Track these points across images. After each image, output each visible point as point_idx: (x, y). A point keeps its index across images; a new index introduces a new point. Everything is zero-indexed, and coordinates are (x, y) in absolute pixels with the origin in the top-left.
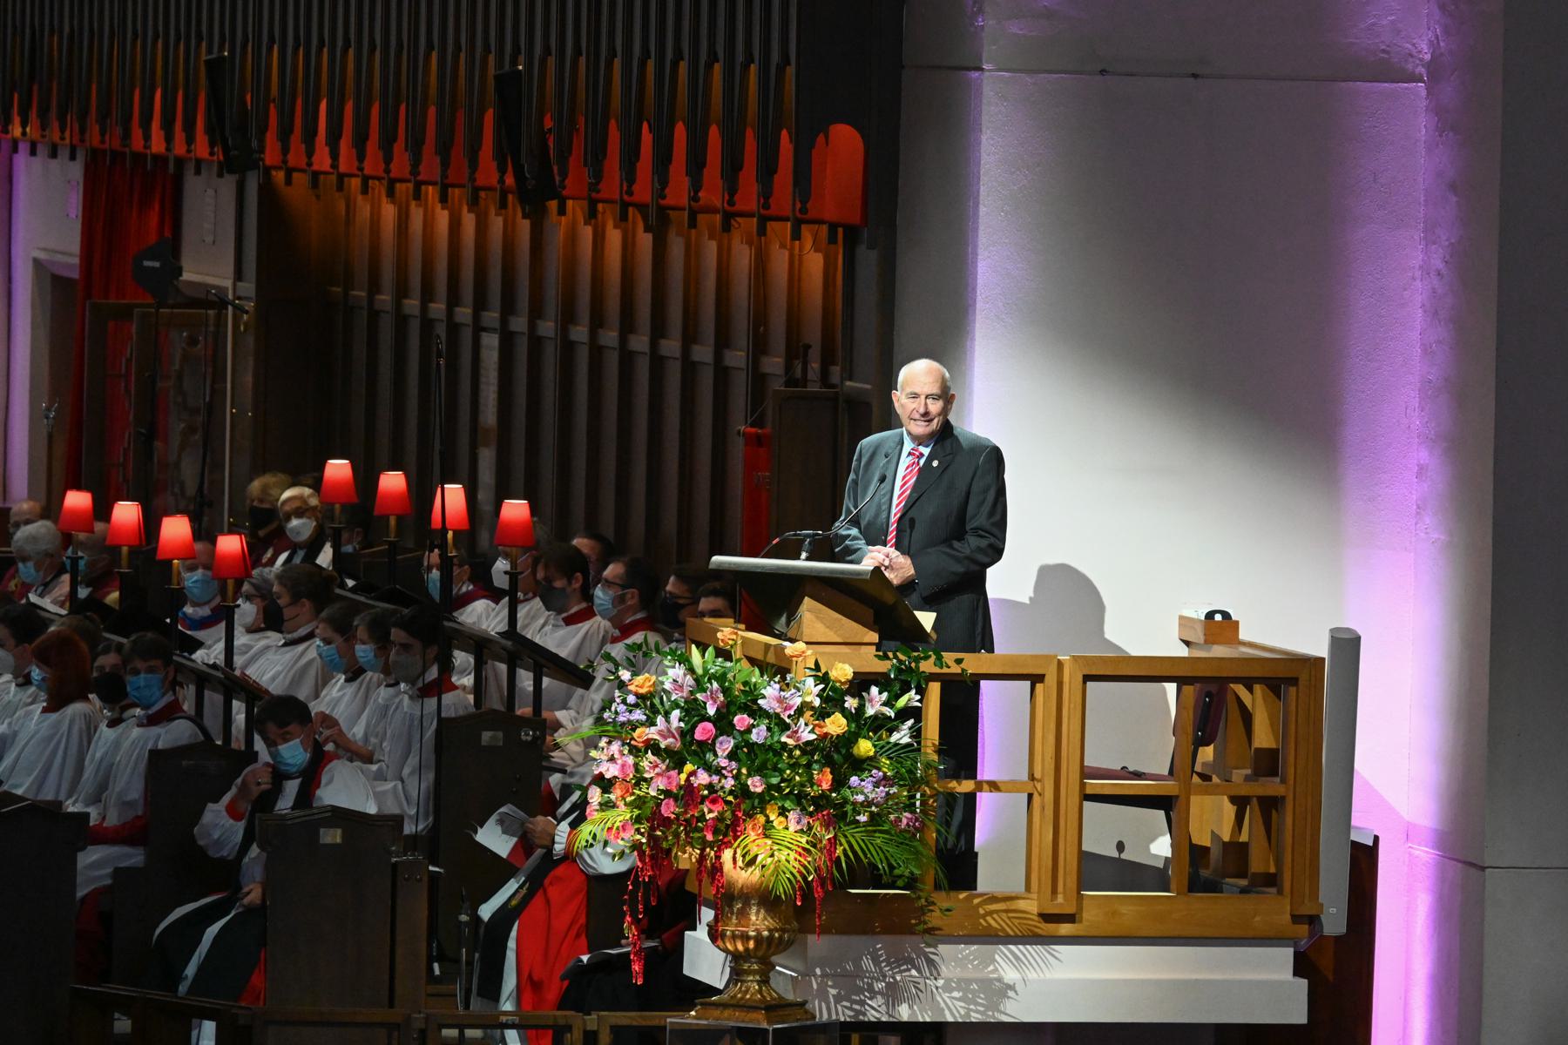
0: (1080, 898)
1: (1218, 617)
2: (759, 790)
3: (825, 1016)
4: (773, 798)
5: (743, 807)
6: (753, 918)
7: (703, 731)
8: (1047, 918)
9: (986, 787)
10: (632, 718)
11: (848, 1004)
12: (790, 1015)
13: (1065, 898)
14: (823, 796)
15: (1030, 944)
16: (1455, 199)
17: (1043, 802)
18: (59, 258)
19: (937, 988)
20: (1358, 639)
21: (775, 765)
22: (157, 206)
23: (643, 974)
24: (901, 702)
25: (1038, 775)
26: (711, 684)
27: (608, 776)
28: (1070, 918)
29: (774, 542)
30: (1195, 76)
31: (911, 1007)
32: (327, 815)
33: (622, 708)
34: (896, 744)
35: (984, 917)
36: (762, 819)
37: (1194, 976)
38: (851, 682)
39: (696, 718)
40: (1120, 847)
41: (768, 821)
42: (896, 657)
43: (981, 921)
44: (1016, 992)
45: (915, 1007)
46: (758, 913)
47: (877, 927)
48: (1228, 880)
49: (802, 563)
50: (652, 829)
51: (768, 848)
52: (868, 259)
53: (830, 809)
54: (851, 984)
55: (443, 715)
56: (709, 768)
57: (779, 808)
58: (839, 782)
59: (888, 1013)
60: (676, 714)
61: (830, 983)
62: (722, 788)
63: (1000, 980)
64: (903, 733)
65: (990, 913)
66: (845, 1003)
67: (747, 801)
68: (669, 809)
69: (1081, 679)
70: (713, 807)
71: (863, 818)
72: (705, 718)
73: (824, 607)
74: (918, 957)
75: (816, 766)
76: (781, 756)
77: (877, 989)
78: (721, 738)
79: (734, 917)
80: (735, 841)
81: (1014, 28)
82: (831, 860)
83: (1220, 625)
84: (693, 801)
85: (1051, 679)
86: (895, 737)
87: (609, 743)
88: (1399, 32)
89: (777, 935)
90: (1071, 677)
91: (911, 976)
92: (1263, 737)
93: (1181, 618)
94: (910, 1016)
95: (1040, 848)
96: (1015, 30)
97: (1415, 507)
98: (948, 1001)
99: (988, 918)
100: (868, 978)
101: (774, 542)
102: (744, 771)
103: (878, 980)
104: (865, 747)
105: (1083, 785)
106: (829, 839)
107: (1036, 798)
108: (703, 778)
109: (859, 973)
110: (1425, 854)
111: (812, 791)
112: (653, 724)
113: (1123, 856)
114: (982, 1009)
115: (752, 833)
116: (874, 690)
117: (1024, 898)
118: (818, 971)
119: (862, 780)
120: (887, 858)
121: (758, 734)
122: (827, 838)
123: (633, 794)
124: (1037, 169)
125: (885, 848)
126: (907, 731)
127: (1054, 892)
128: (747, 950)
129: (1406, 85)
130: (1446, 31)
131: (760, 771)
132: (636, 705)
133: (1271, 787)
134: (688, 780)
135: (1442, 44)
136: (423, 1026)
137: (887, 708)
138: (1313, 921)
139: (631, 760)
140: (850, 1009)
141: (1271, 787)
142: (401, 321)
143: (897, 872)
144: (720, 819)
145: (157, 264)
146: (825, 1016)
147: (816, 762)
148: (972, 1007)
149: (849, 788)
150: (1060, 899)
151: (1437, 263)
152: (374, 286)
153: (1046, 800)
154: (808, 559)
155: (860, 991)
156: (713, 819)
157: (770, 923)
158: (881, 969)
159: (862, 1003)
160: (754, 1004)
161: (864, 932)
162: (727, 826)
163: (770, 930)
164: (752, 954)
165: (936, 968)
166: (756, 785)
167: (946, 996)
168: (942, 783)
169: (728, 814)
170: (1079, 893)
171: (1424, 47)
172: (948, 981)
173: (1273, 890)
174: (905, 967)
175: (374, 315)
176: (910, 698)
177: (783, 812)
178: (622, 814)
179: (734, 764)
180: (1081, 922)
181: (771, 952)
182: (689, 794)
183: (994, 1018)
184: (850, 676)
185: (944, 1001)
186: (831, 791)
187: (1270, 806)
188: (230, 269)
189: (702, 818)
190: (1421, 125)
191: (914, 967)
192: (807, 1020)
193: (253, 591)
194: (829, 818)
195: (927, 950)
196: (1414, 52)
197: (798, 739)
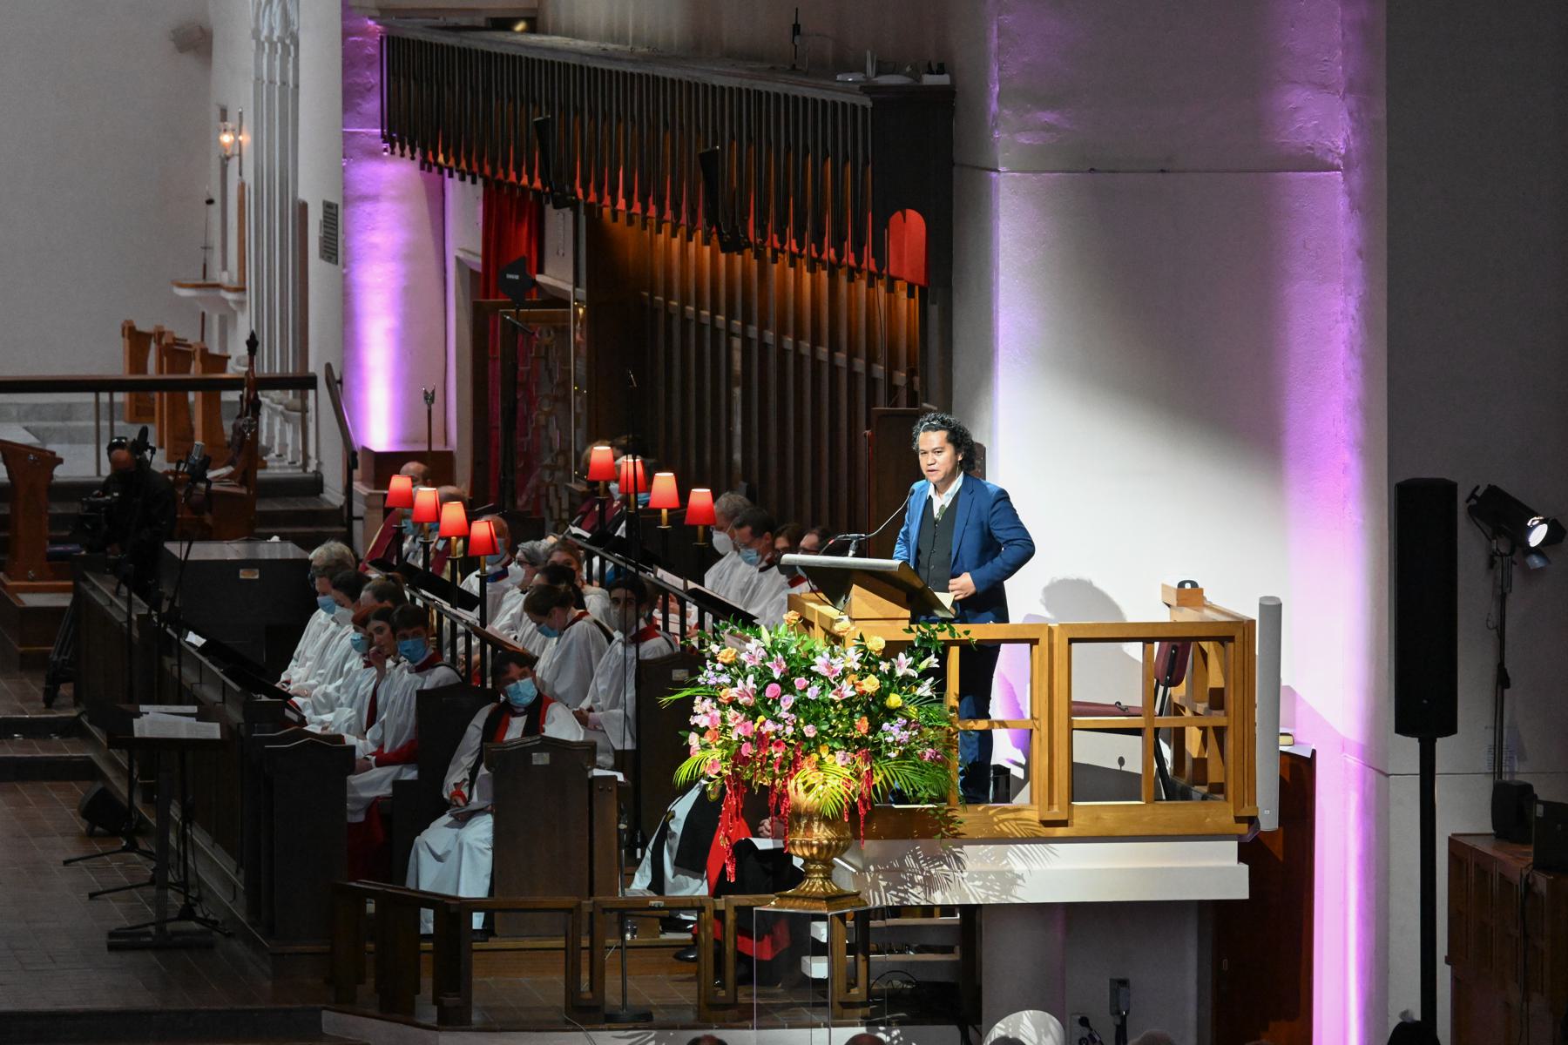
0: (1070, 807)
1: (1188, 586)
2: (812, 735)
3: (878, 903)
4: (824, 741)
5: (802, 748)
6: (816, 830)
7: (772, 690)
8: (1047, 824)
9: (996, 725)
10: (719, 681)
11: (895, 893)
12: (846, 903)
13: (1059, 808)
14: (862, 738)
15: (1034, 843)
16: (1361, 262)
17: (1040, 735)
19: (963, 879)
20: (1280, 606)
21: (826, 716)
22: (526, 224)
23: (736, 873)
24: (923, 665)
25: (1036, 716)
26: (777, 655)
27: (701, 726)
28: (1064, 823)
29: (830, 543)
30: (1163, 171)
31: (943, 893)
32: (537, 743)
33: (711, 674)
34: (920, 697)
35: (997, 824)
36: (815, 757)
37: (1166, 865)
38: (884, 650)
39: (767, 681)
40: (1121, 761)
41: (821, 759)
42: (919, 630)
43: (996, 827)
44: (1024, 881)
45: (947, 894)
46: (819, 827)
47: (916, 834)
48: (1196, 788)
49: (849, 560)
50: (735, 766)
51: (821, 778)
52: (934, 311)
53: (872, 750)
54: (897, 878)
55: (640, 658)
56: (776, 720)
57: (830, 748)
58: (875, 727)
59: (926, 899)
60: (751, 678)
61: (880, 877)
62: (785, 734)
63: (1011, 871)
64: (925, 688)
65: (1003, 821)
66: (892, 892)
67: (805, 744)
68: (748, 750)
69: (1066, 641)
70: (778, 749)
71: (893, 755)
72: (773, 681)
73: (868, 592)
74: (949, 856)
75: (857, 715)
76: (828, 708)
77: (917, 881)
78: (784, 697)
79: (802, 830)
80: (796, 773)
81: (1023, 139)
82: (869, 787)
83: (1189, 593)
84: (763, 744)
85: (1044, 642)
86: (919, 692)
87: (703, 700)
88: (1321, 132)
89: (834, 843)
90: (1060, 642)
91: (942, 870)
92: (1215, 679)
93: (1164, 586)
94: (943, 900)
95: (1039, 771)
96: (1023, 140)
97: (1342, 495)
98: (971, 887)
99: (1001, 825)
100: (910, 872)
101: (830, 543)
102: (802, 720)
103: (918, 874)
104: (894, 700)
105: (1070, 722)
106: (867, 771)
107: (1035, 731)
108: (770, 727)
109: (903, 868)
110: (1353, 761)
111: (856, 735)
112: (735, 686)
113: (1124, 768)
114: (997, 894)
115: (808, 768)
116: (901, 656)
117: (1028, 810)
118: (872, 868)
119: (892, 726)
120: (912, 786)
121: (812, 692)
122: (865, 770)
123: (721, 739)
124: (1043, 246)
125: (911, 776)
126: (928, 686)
127: (1051, 803)
128: (812, 854)
129: (1326, 173)
130: (1353, 133)
131: (814, 720)
132: (723, 671)
133: (1218, 719)
134: (759, 728)
135: (1351, 143)
136: (591, 910)
137: (913, 671)
138: (1252, 821)
139: (718, 713)
140: (896, 896)
141: (1218, 719)
143: (919, 795)
144: (785, 757)
145: (517, 277)
146: (878, 903)
147: (857, 712)
148: (990, 892)
149: (883, 731)
150: (1056, 809)
151: (1352, 311)
152: (668, 296)
153: (1042, 735)
154: (854, 556)
155: (905, 882)
156: (780, 757)
157: (829, 834)
158: (920, 865)
159: (906, 892)
160: (819, 896)
161: (905, 837)
162: (790, 762)
163: (828, 840)
164: (816, 857)
165: (962, 864)
166: (810, 731)
167: (970, 884)
168: (963, 722)
169: (790, 754)
170: (1069, 804)
171: (1341, 144)
172: (971, 873)
173: (1221, 797)
174: (938, 863)
175: (669, 317)
176: (932, 661)
177: (832, 751)
178: (716, 754)
179: (793, 716)
180: (1072, 825)
181: (830, 855)
182: (761, 740)
183: (1007, 900)
184: (883, 645)
185: (968, 888)
186: (869, 733)
187: (1220, 732)
188: (570, 278)
189: (770, 757)
190: (1342, 204)
191: (945, 863)
192: (860, 906)
193: (523, 558)
194: (867, 755)
195: (955, 850)
196: (1333, 148)
197: (842, 696)
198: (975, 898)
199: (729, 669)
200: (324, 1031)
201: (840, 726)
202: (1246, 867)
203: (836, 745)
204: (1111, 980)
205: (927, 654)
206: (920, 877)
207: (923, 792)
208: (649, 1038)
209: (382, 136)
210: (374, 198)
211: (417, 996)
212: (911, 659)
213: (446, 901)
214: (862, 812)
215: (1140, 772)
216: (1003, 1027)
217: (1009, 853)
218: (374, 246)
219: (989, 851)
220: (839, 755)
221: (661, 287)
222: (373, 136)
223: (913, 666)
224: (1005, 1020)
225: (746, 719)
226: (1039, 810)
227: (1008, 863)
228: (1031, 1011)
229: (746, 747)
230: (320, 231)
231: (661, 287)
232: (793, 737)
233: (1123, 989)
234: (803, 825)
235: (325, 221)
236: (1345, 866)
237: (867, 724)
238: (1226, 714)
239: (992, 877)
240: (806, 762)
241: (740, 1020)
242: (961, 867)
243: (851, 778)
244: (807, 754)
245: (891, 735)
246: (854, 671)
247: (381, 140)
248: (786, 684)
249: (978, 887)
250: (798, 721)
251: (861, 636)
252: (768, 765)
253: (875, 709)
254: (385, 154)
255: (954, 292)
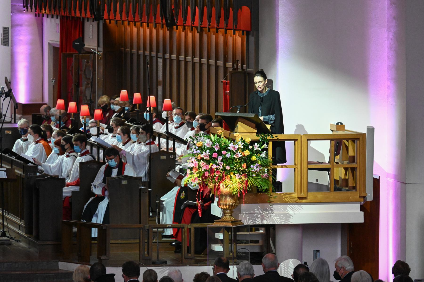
1: (340, 124)
2: (229, 169)
4: (232, 171)
5: (225, 173)
6: (228, 200)
8: (299, 198)
10: (197, 152)
11: (252, 221)
14: (244, 170)
18: (55, 42)
19: (273, 216)
20: (374, 128)
24: (263, 147)
25: (296, 164)
28: (305, 198)
34: (262, 157)
36: (229, 176)
40: (317, 180)
41: (231, 176)
42: (261, 136)
43: (284, 199)
44: (292, 216)
45: (268, 221)
46: (229, 199)
50: (203, 179)
51: (231, 183)
53: (247, 174)
58: (248, 167)
59: (261, 222)
60: (208, 151)
62: (220, 169)
63: (288, 214)
64: (263, 154)
65: (286, 197)
66: (251, 220)
68: (207, 174)
72: (215, 152)
74: (268, 209)
75: (242, 163)
78: (219, 157)
79: (223, 200)
83: (340, 126)
85: (299, 140)
86: (261, 155)
89: (234, 204)
90: (304, 140)
91: (267, 213)
92: (351, 153)
98: (276, 219)
99: (285, 199)
102: (225, 164)
103: (259, 214)
104: (254, 158)
106: (246, 181)
107: (296, 169)
108: (215, 166)
111: (241, 169)
113: (318, 183)
116: (256, 144)
122: (245, 180)
123: (198, 171)
125: (259, 182)
126: (264, 154)
127: (301, 192)
128: (227, 208)
131: (229, 164)
132: (198, 149)
133: (354, 165)
134: (211, 167)
139: (197, 162)
142: (138, 56)
143: (263, 188)
144: (219, 176)
147: (242, 162)
148: (282, 220)
149: (251, 168)
150: (303, 193)
151: (391, 37)
155: (255, 217)
157: (232, 201)
158: (259, 212)
159: (255, 220)
163: (232, 203)
166: (228, 168)
167: (275, 218)
168: (273, 166)
169: (221, 175)
172: (276, 214)
173: (355, 190)
175: (132, 55)
176: (265, 146)
177: (234, 174)
180: (308, 199)
182: (211, 171)
187: (353, 170)
188: (96, 44)
189: (215, 176)
191: (268, 211)
197: (238, 156)
198: (277, 222)
199: (200, 148)
200: (59, 268)
201: (238, 166)
202: (363, 213)
203: (236, 172)
204: (314, 250)
205: (264, 143)
206: (260, 216)
207: (264, 187)
208: (167, 269)
209: (23, 6)
210: (21, 25)
211: (91, 257)
212: (259, 145)
213: (102, 226)
214: (244, 194)
215: (339, 179)
216: (283, 264)
217: (288, 208)
218: (21, 40)
219: (281, 207)
220: (237, 175)
221: (129, 45)
222: (21, 6)
223: (259, 147)
224: (284, 262)
225: (206, 164)
226: (297, 194)
227: (288, 211)
228: (292, 259)
229: (206, 173)
230: (2, 36)
231: (129, 45)
232: (222, 170)
233: (318, 253)
234: (224, 198)
235: (3, 33)
236: (388, 214)
237: (246, 165)
238: (356, 164)
239: (282, 215)
240: (226, 177)
241: (195, 264)
242: (273, 213)
243: (241, 182)
244: (226, 175)
245: (254, 169)
246: (241, 149)
247: (23, 7)
248: (219, 153)
249: (278, 219)
250: (224, 164)
251: (242, 138)
252: (214, 179)
253: (248, 160)
254: (24, 11)
255: (260, 32)
